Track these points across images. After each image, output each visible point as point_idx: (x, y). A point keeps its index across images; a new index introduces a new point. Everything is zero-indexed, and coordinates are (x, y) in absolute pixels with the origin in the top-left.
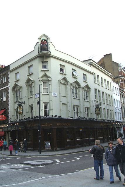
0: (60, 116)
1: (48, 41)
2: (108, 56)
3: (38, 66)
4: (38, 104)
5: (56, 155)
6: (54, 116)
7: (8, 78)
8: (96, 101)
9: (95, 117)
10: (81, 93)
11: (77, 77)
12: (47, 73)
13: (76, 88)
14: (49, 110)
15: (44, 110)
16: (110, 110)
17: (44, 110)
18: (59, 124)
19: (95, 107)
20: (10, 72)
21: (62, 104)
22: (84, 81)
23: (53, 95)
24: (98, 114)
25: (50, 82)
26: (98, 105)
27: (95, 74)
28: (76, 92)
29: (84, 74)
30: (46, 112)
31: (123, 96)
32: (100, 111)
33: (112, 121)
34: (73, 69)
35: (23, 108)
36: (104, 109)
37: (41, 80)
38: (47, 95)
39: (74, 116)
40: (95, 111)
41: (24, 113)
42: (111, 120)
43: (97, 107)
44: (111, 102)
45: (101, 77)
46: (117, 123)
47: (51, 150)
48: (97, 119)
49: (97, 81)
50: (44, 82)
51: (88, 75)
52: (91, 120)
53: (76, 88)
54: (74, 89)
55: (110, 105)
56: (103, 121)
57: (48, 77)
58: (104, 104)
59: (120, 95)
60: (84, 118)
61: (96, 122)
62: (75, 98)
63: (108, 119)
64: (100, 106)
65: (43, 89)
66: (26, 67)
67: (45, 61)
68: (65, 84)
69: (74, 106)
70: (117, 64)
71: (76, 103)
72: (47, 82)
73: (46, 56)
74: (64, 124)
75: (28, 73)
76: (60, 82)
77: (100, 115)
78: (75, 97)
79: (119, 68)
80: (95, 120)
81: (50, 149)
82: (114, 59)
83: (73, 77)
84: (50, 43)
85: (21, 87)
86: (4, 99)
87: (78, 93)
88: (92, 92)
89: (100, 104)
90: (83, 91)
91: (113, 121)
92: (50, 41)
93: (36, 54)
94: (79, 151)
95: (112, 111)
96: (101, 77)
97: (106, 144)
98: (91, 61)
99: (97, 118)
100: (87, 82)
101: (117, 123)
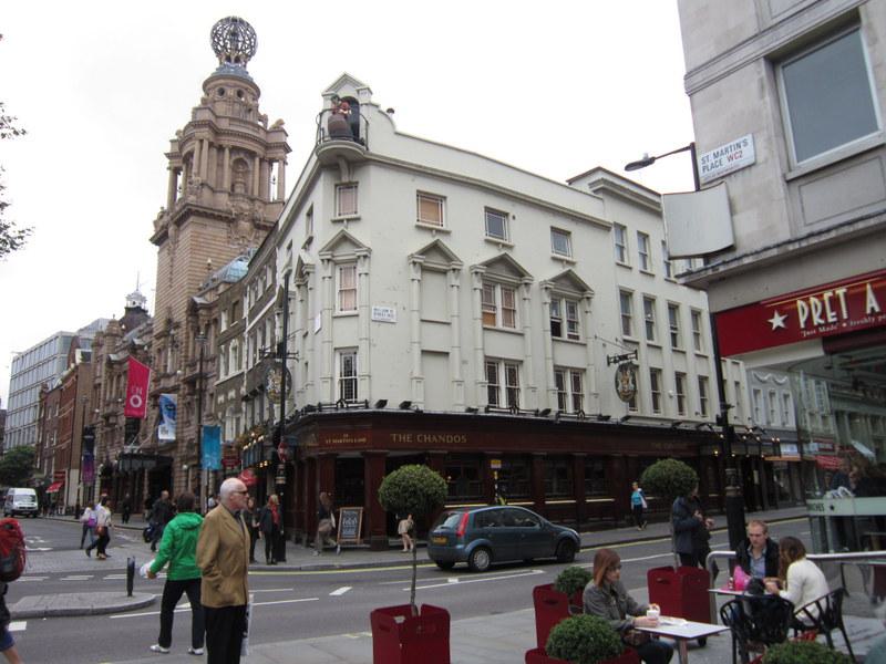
0: (406, 405)
1: (362, 99)
9: (617, 411)
10: (534, 312)
13: (509, 292)
15: (341, 381)
17: (337, 378)
18: (406, 438)
21: (424, 352)
23: (379, 318)
29: (554, 230)
32: (634, 382)
36: (680, 377)
37: (329, 257)
40: (617, 385)
43: (626, 366)
45: (639, 233)
47: (364, 545)
50: (342, 266)
51: (580, 235)
53: (509, 292)
54: (498, 292)
56: (669, 425)
57: (355, 244)
58: (735, 366)
62: (563, 341)
67: (345, 179)
68: (444, 273)
71: (503, 347)
72: (353, 265)
78: (500, 324)
81: (358, 540)
84: (371, 108)
89: (636, 352)
92: (374, 100)
96: (639, 233)
97: (407, 536)
98: (600, 176)
99: (631, 413)
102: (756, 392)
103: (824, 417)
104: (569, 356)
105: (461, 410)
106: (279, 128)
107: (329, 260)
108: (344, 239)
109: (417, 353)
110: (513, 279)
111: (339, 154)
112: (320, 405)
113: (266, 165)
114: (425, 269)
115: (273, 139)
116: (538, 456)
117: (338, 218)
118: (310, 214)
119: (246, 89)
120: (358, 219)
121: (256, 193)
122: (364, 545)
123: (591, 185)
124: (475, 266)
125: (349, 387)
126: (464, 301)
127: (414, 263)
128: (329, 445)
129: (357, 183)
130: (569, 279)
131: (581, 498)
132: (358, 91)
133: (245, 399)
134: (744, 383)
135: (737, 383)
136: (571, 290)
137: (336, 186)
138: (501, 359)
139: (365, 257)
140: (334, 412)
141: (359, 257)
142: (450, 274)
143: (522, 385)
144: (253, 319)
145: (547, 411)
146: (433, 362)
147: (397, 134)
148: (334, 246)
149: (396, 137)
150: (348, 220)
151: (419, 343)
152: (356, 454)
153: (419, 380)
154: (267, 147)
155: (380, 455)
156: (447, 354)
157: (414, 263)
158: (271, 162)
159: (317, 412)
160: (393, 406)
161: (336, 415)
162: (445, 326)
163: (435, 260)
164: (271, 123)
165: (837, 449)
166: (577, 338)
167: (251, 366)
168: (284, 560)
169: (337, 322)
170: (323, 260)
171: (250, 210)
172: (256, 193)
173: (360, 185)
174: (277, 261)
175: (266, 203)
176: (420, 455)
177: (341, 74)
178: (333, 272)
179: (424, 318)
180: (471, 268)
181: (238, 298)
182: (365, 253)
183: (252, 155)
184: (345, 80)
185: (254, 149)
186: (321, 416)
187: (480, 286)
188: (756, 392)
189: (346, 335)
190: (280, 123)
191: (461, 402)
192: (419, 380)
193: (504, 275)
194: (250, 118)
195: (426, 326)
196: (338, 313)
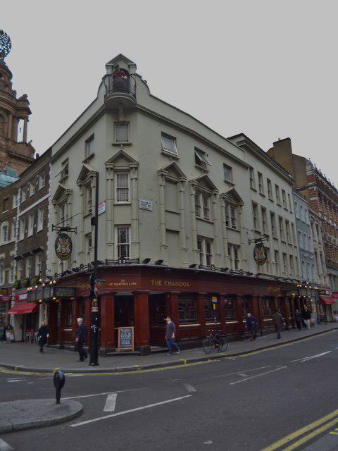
0: (160, 262)
2: (284, 144)
3: (103, 130)
4: (92, 224)
5: (135, 369)
6: (141, 260)
7: (48, 178)
8: (256, 232)
10: (218, 210)
11: (209, 168)
12: (127, 151)
13: (206, 196)
14: (130, 243)
16: (291, 256)
17: (116, 244)
18: (159, 283)
19: (253, 245)
20: (53, 163)
21: (168, 231)
22: (225, 182)
24: (260, 262)
25: (134, 174)
26: (260, 240)
27: (252, 169)
28: (206, 203)
30: (123, 251)
31: (317, 227)
32: (266, 254)
33: (295, 282)
34: (196, 149)
35: (71, 243)
37: (112, 166)
38: (126, 207)
39: (198, 263)
40: (255, 255)
41: (75, 256)
42: (293, 278)
44: (292, 239)
45: (259, 173)
46: (307, 285)
47: (136, 352)
48: (259, 274)
49: (257, 183)
50: (119, 173)
51: (236, 170)
52: (245, 275)
55: (289, 244)
56: (273, 279)
57: (129, 160)
59: (312, 224)
60: (227, 269)
61: (257, 281)
63: (286, 277)
64: (266, 244)
65: (115, 191)
66: (82, 142)
67: (122, 119)
68: (176, 183)
69: (200, 238)
70: (303, 161)
72: (125, 173)
73: (124, 109)
74: (170, 284)
75: (84, 156)
76: (161, 174)
77: (265, 264)
79: (308, 168)
80: (253, 276)
82: (296, 150)
83: (196, 167)
85: (70, 193)
86: (40, 227)
87: (209, 208)
88: (247, 209)
90: (224, 205)
91: (299, 281)
92: (138, 72)
93: (101, 103)
94: (314, 333)
95: (294, 258)
96: (259, 173)
100: (233, 185)
101: (307, 285)
102: (303, 262)
103: (324, 278)
104: (234, 238)
105: (186, 267)
106: (24, 98)
107: (111, 169)
108: (122, 156)
109: (164, 231)
110: (208, 191)
111: (120, 102)
112: (106, 260)
113: (16, 120)
114: (168, 181)
115: (21, 105)
116: (201, 295)
117: (115, 142)
118: (92, 138)
119: (5, 73)
120: (130, 145)
121: (9, 136)
122: (136, 352)
123: (238, 143)
124: (192, 181)
125: (123, 251)
126: (186, 200)
127: (162, 175)
128: (111, 287)
129: (129, 122)
130: (233, 194)
131: (203, 323)
132: (129, 67)
133: (18, 259)
134: (299, 258)
135: (296, 258)
136: (234, 200)
137: (115, 123)
138: (203, 237)
139: (136, 168)
140: (117, 265)
141: (132, 168)
142: (180, 184)
143: (213, 253)
144: (25, 208)
145: (193, 266)
146: (172, 236)
147: (151, 96)
148: (115, 159)
149: (150, 98)
150: (124, 145)
151: (165, 224)
152: (129, 293)
153: (166, 247)
154: (17, 109)
155: (146, 293)
156: (178, 232)
157: (162, 175)
158: (19, 118)
159: (105, 265)
160: (152, 264)
161: (117, 267)
162: (177, 216)
163: (172, 174)
164: (18, 97)
165: (331, 294)
166: (235, 227)
167: (22, 237)
168: (98, 365)
169: (116, 208)
170: (107, 169)
171: (7, 146)
172: (9, 136)
173: (131, 124)
174: (50, 172)
175: (15, 143)
176: (163, 294)
177: (118, 54)
178: (114, 177)
179: (168, 209)
180: (189, 182)
181: (9, 196)
182: (135, 166)
183: (8, 113)
184: (121, 58)
185: (9, 109)
186: (107, 268)
187: (194, 193)
188: (303, 262)
189: (122, 217)
190: (25, 96)
191: (187, 262)
192: (166, 247)
193: (205, 187)
194: (7, 90)
195: (169, 214)
196: (116, 203)
